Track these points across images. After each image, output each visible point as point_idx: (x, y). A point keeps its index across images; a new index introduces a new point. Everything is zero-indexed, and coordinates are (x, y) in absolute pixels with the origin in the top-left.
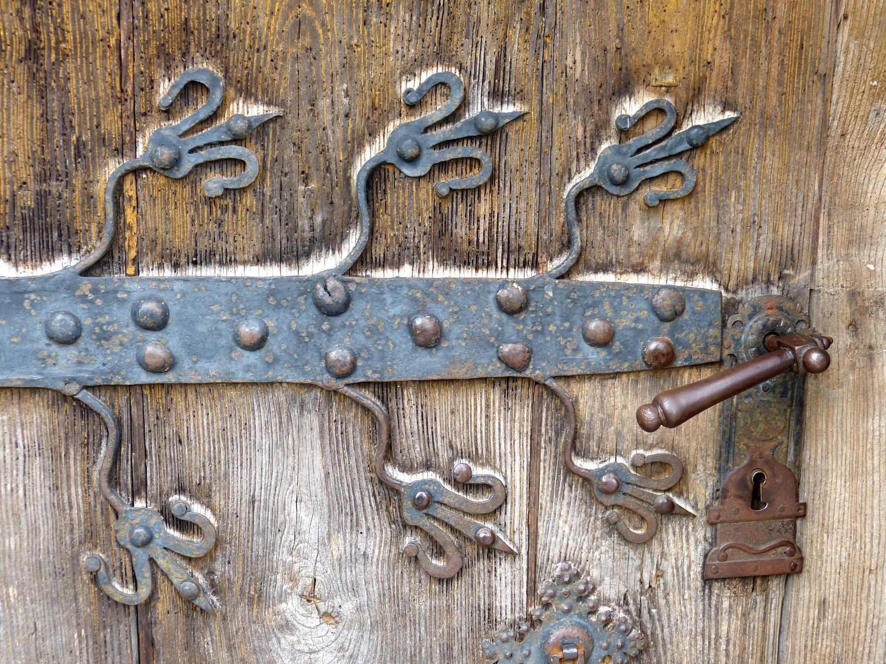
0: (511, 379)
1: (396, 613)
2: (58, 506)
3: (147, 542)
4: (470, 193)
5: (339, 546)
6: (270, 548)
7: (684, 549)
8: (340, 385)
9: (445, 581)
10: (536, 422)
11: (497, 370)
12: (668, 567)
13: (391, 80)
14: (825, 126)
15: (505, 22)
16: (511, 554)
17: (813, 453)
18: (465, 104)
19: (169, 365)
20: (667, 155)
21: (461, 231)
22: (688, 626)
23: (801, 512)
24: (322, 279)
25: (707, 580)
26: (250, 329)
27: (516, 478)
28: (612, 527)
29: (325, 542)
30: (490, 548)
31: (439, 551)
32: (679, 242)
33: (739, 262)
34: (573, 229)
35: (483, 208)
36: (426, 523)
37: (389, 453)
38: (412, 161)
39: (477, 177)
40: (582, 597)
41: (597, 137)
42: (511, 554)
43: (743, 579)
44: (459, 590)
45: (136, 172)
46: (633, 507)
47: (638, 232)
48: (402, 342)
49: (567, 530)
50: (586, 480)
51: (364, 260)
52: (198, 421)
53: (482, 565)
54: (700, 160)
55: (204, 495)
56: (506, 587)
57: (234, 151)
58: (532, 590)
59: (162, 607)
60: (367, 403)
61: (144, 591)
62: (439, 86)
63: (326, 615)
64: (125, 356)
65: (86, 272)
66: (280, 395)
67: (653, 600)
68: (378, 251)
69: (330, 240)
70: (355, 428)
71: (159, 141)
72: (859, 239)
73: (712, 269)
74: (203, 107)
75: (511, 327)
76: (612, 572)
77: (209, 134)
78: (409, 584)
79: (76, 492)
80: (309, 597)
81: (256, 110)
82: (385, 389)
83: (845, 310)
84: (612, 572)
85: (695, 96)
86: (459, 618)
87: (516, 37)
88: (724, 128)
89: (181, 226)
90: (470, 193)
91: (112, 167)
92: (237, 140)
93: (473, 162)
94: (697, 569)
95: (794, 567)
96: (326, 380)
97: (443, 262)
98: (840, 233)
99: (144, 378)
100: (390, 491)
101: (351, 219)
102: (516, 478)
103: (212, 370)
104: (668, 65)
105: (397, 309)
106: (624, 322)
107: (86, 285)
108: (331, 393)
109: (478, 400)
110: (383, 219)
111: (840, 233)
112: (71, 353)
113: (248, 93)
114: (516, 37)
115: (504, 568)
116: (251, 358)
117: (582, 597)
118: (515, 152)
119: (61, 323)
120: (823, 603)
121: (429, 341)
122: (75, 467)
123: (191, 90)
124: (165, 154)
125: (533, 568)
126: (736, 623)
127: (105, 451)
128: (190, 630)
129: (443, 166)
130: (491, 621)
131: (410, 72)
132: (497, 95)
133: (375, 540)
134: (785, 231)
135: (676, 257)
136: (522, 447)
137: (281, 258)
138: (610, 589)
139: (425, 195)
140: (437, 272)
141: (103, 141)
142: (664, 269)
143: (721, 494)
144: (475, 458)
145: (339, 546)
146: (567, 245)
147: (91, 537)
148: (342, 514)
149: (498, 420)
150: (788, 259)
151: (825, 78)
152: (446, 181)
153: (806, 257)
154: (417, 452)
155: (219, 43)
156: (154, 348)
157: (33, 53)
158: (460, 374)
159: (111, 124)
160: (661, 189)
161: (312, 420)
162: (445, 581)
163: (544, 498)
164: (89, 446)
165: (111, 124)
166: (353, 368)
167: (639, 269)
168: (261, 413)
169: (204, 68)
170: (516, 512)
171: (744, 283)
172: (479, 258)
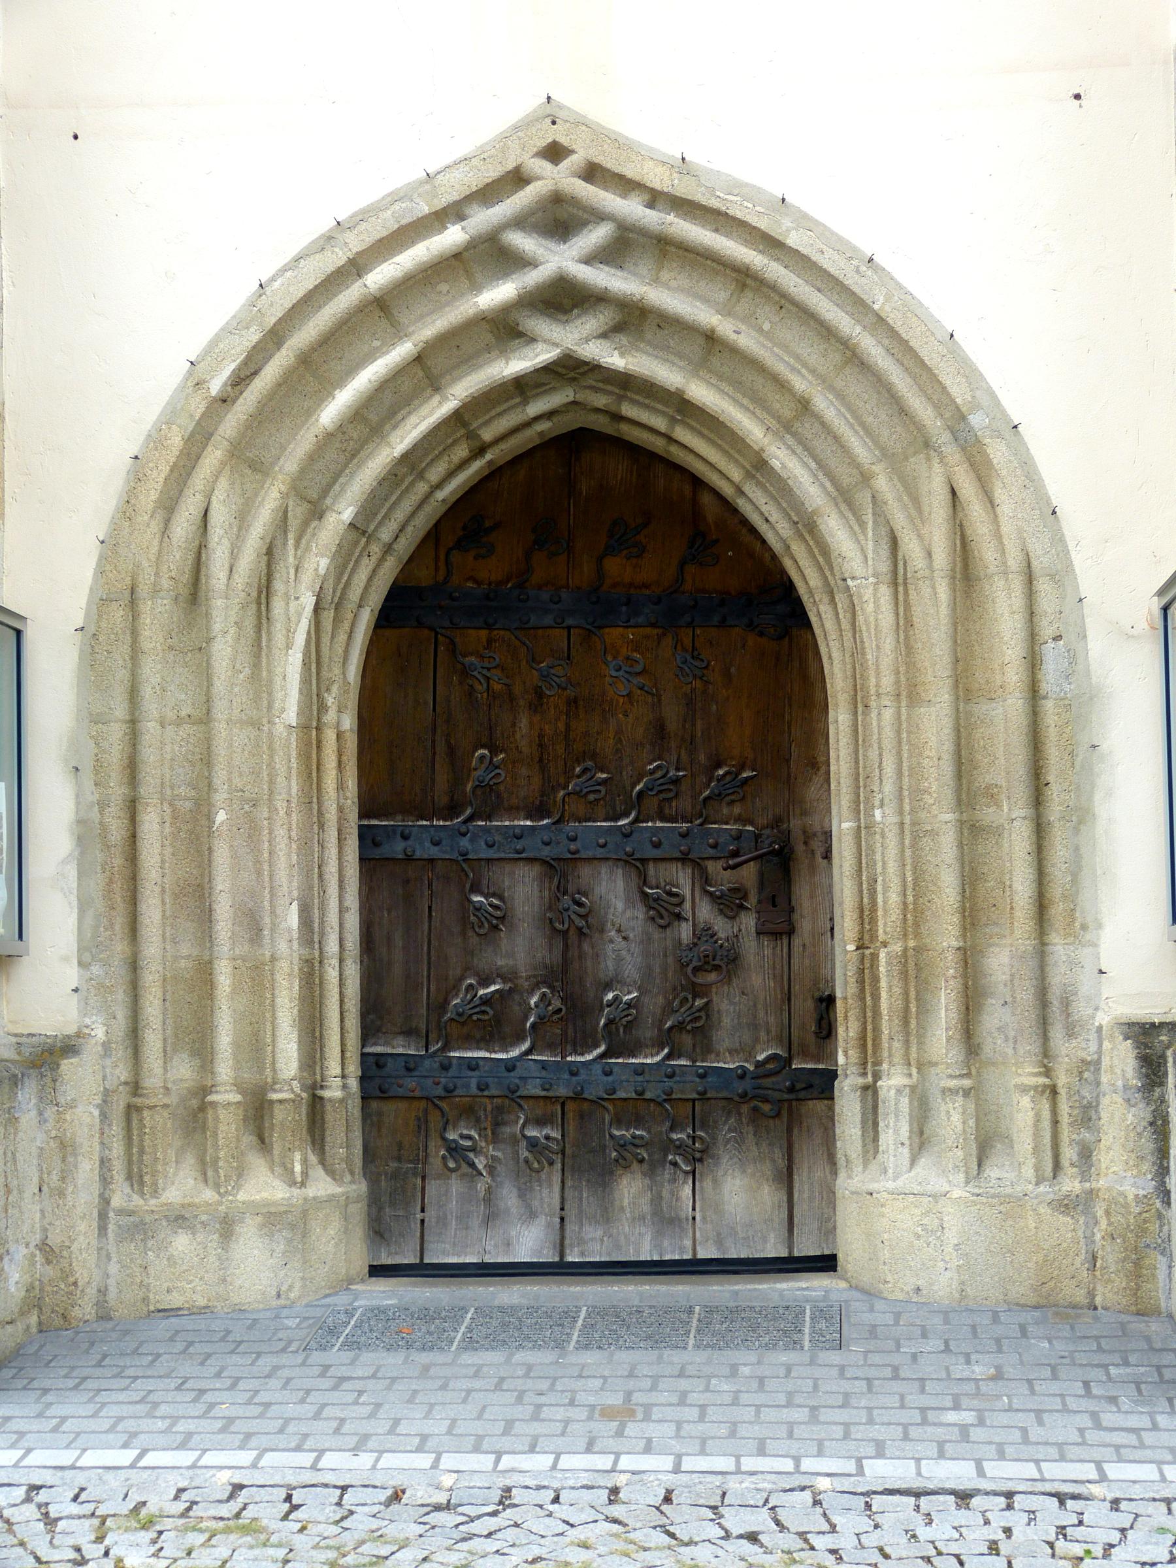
0: (684, 859)
1: (647, 940)
2: (541, 898)
3: (568, 909)
4: (669, 800)
5: (628, 914)
6: (606, 913)
7: (748, 921)
8: (629, 859)
9: (664, 927)
10: (693, 874)
11: (678, 855)
12: (743, 927)
13: (645, 766)
14: (789, 775)
15: (680, 747)
16: (686, 920)
17: (795, 889)
18: (667, 772)
19: (577, 852)
20: (1044, 687)
21: (667, 811)
22: (752, 951)
23: (792, 910)
24: (623, 825)
25: (758, 933)
26: (602, 841)
27: (687, 892)
28: (721, 911)
29: (624, 912)
30: (679, 917)
31: (662, 917)
32: (740, 815)
33: (762, 821)
34: (703, 812)
35: (674, 804)
36: (657, 906)
37: (645, 883)
38: (651, 790)
39: (671, 795)
40: (712, 936)
41: (710, 781)
42: (686, 920)
43: (772, 934)
44: (668, 931)
45: (569, 794)
46: (730, 903)
47: (725, 811)
48: (649, 846)
49: (705, 912)
50: (711, 894)
51: (636, 821)
52: (586, 871)
53: (676, 923)
54: (745, 788)
55: (586, 895)
56: (685, 932)
57: (598, 788)
58: (694, 931)
59: (571, 933)
60: (637, 865)
61: (566, 926)
62: (658, 767)
63: (625, 938)
64: (561, 849)
65: (554, 824)
66: (610, 863)
67: (738, 941)
68: (641, 818)
69: (626, 814)
70: (634, 875)
71: (576, 785)
72: (805, 813)
73: (752, 824)
74: (589, 775)
75: (684, 841)
76: (722, 928)
77: (591, 783)
78: (652, 928)
79: (547, 893)
80: (619, 931)
81: (604, 776)
82: (644, 861)
83: (802, 838)
84: (722, 928)
85: (742, 768)
86: (669, 943)
87: (683, 751)
88: (752, 777)
89: (581, 810)
90: (669, 800)
91: (562, 793)
92: (599, 784)
93: (670, 790)
94: (753, 929)
95: (791, 932)
96: (625, 857)
97: (662, 821)
98: (798, 811)
99: (570, 856)
100: (645, 895)
101: (632, 808)
102: (687, 892)
103: (590, 854)
104: (732, 758)
105: (648, 835)
106: (721, 840)
107: (553, 828)
108: (626, 862)
109: (673, 867)
110: (643, 808)
111: (798, 811)
112: (548, 848)
113: (603, 772)
114: (683, 751)
115: (684, 924)
116: (602, 850)
117: (712, 936)
118: (684, 787)
119: (546, 838)
120: (804, 945)
121: (657, 845)
122: (547, 885)
123: (585, 771)
124: (578, 789)
125: (694, 925)
126: (771, 951)
127: (556, 881)
128: (580, 941)
129: (660, 792)
130: (680, 943)
131: (651, 764)
132: (678, 769)
133: (640, 913)
134: (777, 811)
135: (739, 819)
136: (689, 882)
137: (611, 820)
138: (721, 935)
139: (655, 801)
140: (659, 824)
141: (559, 785)
142: (734, 824)
143: (759, 902)
144: (674, 886)
145: (628, 914)
146: (701, 816)
147: (550, 908)
148: (629, 903)
149: (681, 874)
150: (777, 821)
151: (788, 761)
152: (661, 796)
153: (786, 820)
154: (654, 882)
155: (594, 756)
156: (573, 847)
157: (541, 760)
158: (667, 856)
159: (562, 780)
160: (733, 797)
161: (620, 871)
162: (664, 927)
163: (697, 900)
164: (551, 878)
165: (562, 780)
166: (633, 854)
167: (727, 823)
168: (604, 869)
169: (590, 763)
170: (688, 905)
171: (763, 828)
172: (673, 819)
